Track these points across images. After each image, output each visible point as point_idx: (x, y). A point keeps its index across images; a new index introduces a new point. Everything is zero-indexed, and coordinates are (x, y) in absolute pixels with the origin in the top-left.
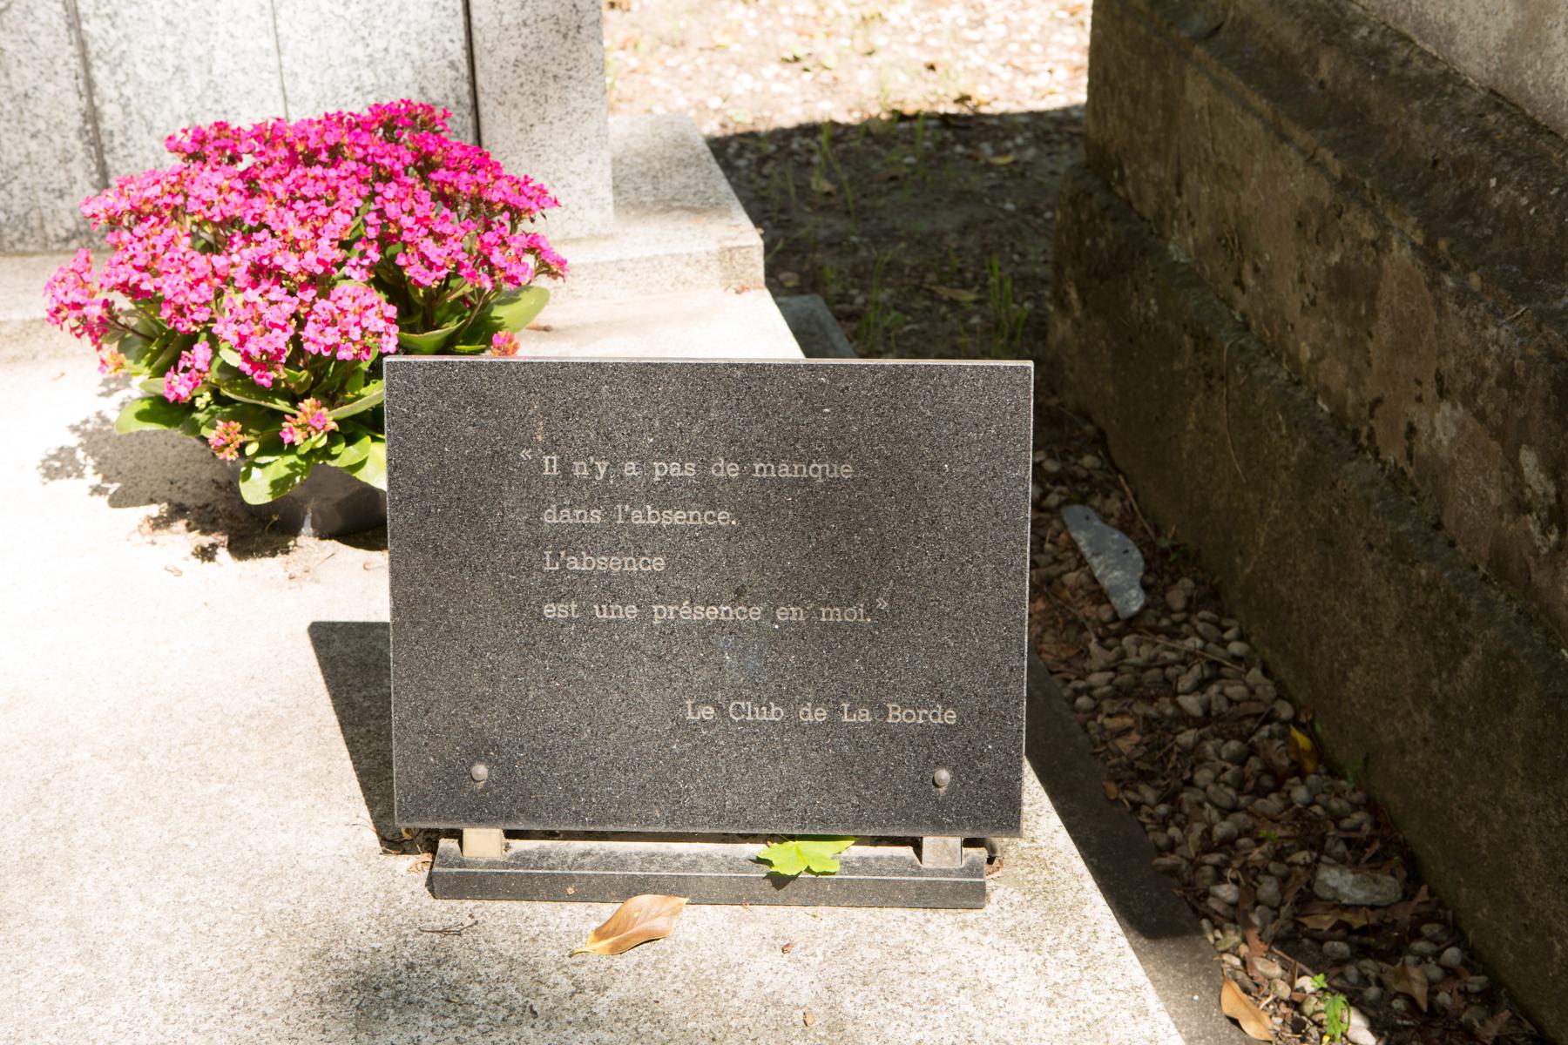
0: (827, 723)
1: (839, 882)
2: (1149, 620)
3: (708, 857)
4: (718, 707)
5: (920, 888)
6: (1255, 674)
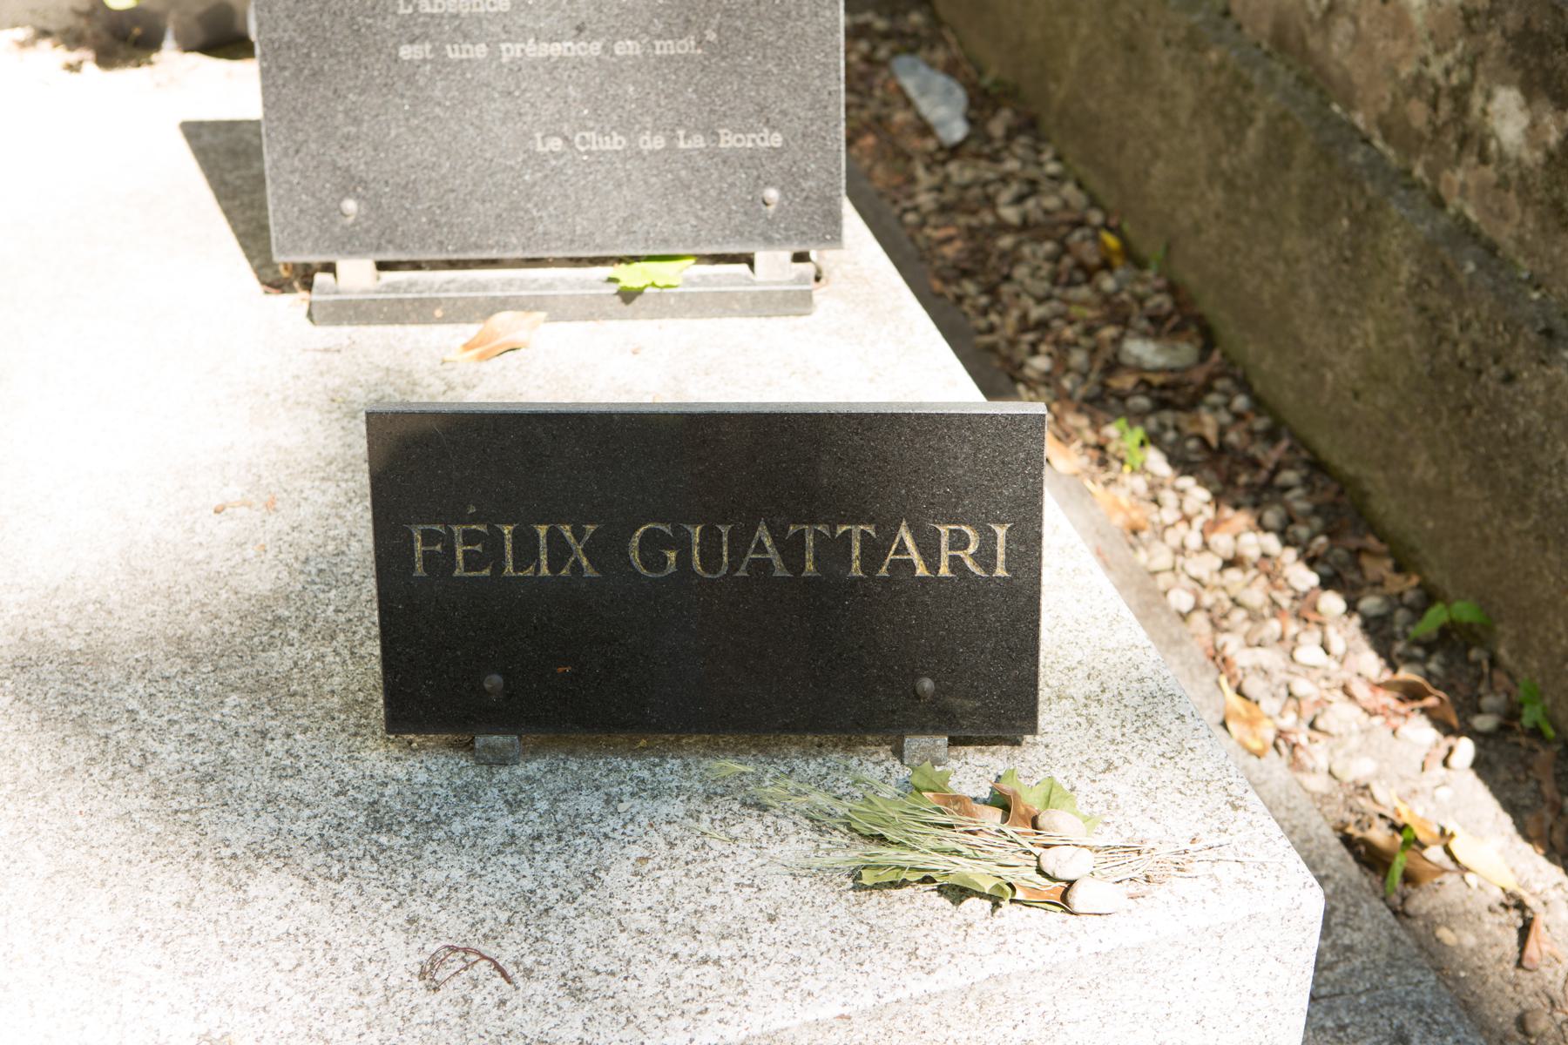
0: (665, 149)
1: (682, 295)
2: (973, 146)
3: (563, 280)
4: (566, 139)
5: (755, 297)
6: (1069, 189)
